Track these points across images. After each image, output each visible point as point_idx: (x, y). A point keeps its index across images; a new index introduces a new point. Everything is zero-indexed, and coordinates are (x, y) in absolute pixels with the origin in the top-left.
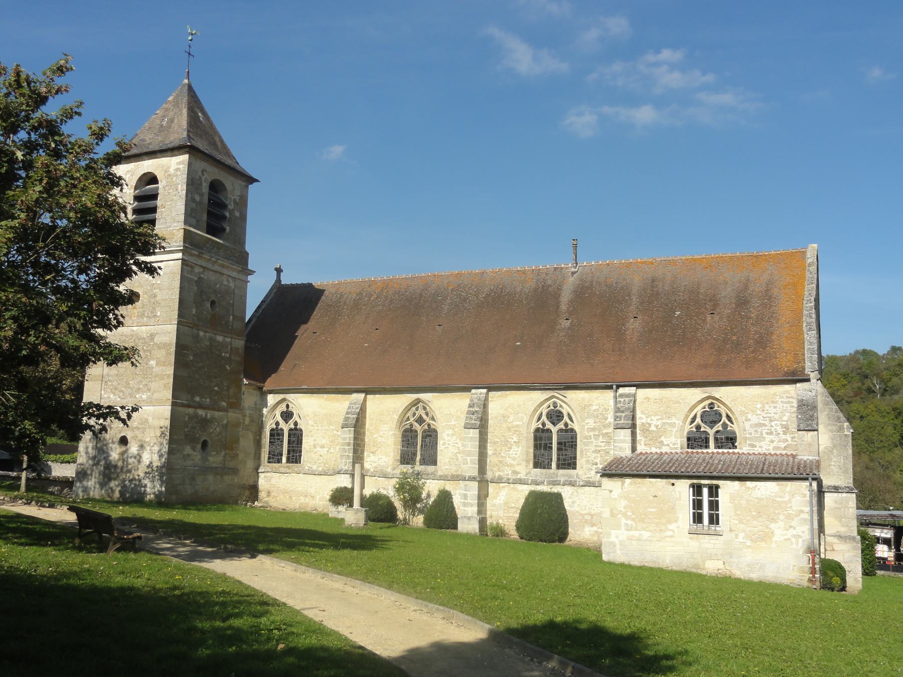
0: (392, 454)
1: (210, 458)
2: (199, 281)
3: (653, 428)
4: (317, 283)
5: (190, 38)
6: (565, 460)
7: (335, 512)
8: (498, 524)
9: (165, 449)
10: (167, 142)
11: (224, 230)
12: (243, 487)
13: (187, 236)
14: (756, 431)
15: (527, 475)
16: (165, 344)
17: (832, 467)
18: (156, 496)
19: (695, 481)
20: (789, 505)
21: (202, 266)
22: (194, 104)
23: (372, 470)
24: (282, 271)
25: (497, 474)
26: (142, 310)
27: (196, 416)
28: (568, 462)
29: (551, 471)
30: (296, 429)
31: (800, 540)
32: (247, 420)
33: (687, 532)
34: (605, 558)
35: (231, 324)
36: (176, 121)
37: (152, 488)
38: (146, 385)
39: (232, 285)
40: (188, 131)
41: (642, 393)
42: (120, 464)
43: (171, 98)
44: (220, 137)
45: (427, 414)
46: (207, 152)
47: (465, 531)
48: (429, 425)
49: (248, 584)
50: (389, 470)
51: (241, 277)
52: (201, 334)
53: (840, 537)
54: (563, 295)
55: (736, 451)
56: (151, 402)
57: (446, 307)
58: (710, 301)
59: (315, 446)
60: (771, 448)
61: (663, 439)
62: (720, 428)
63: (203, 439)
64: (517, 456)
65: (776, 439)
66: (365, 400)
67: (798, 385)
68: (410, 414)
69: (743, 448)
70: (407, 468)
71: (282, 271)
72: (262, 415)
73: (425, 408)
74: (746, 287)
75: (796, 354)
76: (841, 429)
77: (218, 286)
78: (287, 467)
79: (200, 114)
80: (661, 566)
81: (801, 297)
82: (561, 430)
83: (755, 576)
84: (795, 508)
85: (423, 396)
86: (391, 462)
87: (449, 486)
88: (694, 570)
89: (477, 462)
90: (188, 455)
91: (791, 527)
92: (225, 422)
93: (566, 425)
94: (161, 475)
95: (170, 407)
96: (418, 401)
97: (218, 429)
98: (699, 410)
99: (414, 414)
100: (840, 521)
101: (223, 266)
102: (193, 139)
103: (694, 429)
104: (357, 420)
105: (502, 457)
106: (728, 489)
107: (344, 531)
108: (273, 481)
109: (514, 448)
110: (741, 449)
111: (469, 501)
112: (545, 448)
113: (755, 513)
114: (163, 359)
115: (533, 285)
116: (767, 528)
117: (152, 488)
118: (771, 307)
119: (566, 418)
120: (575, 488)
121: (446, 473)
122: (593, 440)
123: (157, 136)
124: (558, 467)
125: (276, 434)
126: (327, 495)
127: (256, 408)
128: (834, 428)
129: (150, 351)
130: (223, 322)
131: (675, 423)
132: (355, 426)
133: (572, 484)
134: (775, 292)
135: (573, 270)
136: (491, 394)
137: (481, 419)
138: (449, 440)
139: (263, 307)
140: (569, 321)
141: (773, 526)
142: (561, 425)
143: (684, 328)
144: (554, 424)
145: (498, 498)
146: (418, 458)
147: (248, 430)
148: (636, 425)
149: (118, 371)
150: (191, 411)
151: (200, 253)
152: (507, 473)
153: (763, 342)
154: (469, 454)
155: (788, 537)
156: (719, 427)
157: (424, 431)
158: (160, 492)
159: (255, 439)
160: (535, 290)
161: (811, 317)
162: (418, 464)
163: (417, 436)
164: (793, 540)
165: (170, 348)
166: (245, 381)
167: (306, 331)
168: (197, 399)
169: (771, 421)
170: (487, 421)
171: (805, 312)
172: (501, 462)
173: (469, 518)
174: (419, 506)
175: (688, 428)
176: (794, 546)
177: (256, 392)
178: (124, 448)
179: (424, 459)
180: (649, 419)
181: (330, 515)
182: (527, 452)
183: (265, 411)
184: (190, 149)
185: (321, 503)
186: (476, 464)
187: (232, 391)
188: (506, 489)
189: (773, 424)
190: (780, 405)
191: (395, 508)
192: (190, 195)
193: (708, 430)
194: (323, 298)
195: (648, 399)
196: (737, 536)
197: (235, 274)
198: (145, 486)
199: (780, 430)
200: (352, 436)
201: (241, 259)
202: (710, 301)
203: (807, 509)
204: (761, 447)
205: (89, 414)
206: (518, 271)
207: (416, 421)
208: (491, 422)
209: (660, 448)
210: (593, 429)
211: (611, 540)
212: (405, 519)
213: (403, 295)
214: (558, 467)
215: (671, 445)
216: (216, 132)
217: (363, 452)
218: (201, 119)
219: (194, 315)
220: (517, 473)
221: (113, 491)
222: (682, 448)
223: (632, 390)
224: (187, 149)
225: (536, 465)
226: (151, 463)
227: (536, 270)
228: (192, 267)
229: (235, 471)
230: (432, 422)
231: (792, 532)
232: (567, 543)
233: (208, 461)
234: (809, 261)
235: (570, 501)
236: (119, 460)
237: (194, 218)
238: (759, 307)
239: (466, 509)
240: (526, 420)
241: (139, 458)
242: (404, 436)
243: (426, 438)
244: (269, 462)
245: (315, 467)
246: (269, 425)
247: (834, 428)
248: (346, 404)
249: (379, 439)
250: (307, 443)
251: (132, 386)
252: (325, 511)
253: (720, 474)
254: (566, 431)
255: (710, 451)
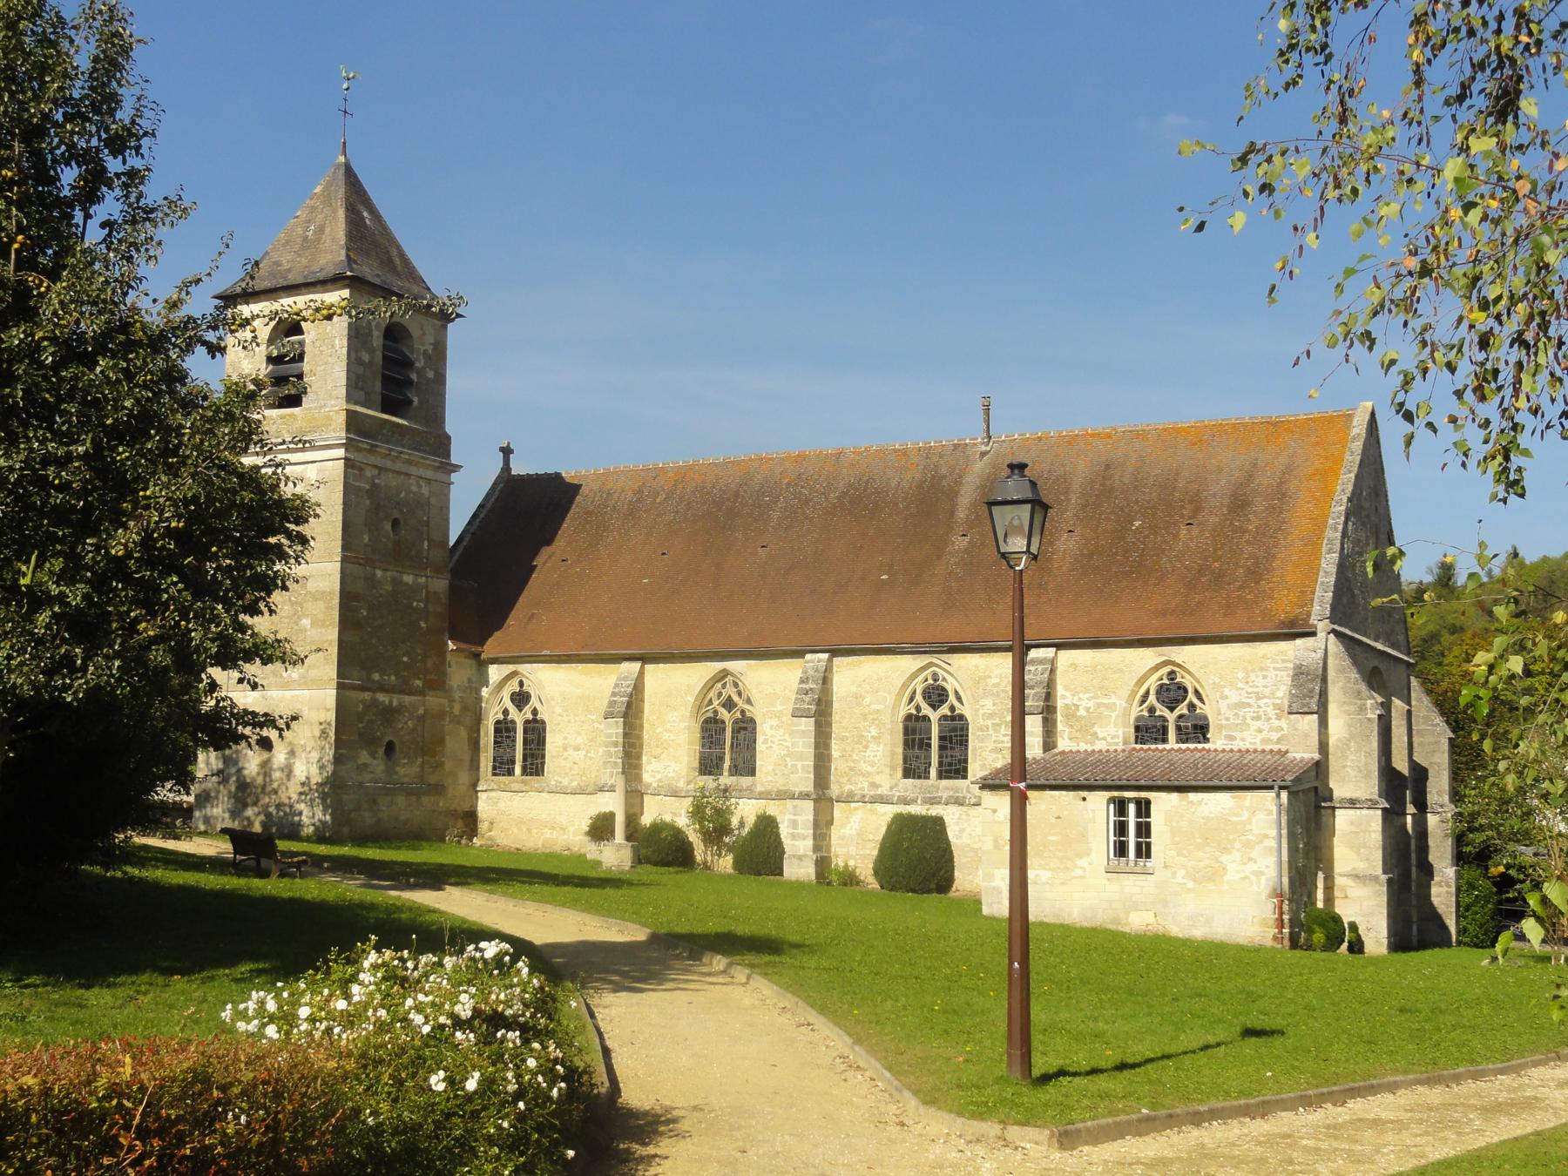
0: (685, 759)
1: (398, 769)
2: (373, 491)
3: (1082, 712)
4: (569, 474)
5: (345, 86)
6: (950, 764)
7: (592, 851)
8: (846, 866)
9: (330, 753)
10: (315, 268)
11: (410, 402)
12: (453, 814)
13: (353, 422)
14: (1236, 714)
15: (891, 788)
17: (1348, 769)
18: (317, 828)
19: (1116, 794)
20: (1248, 827)
21: (375, 467)
22: (356, 196)
23: (655, 785)
24: (512, 451)
25: (846, 788)
27: (375, 702)
28: (955, 768)
29: (930, 782)
30: (535, 720)
31: (1263, 879)
32: (457, 709)
33: (1103, 870)
34: (986, 910)
35: (425, 554)
36: (327, 230)
37: (311, 816)
39: (425, 491)
40: (348, 249)
41: (1066, 657)
42: (260, 780)
43: (318, 189)
44: (399, 247)
45: (740, 694)
46: (377, 281)
47: (794, 879)
48: (743, 712)
50: (681, 784)
51: (440, 476)
52: (379, 573)
53: (1356, 877)
54: (962, 492)
55: (1207, 746)
56: (305, 683)
57: (776, 515)
58: (1191, 502)
59: (565, 748)
60: (1258, 741)
61: (1096, 728)
62: (1185, 711)
63: (387, 739)
64: (876, 760)
65: (1266, 727)
66: (641, 673)
67: (1299, 642)
68: (712, 694)
69: (1217, 742)
70: (709, 782)
71: (512, 451)
72: (479, 699)
73: (736, 685)
74: (1250, 477)
75: (1302, 592)
76: (1362, 709)
77: (402, 495)
78: (523, 782)
79: (365, 214)
80: (1067, 920)
81: (1329, 495)
82: (944, 717)
83: (1198, 933)
84: (1256, 831)
85: (733, 665)
86: (684, 772)
87: (773, 809)
88: (1112, 927)
89: (812, 770)
90: (366, 765)
91: (1250, 859)
92: (421, 711)
93: (952, 708)
94: (324, 797)
95: (338, 565)
96: (725, 673)
97: (410, 723)
98: (1152, 683)
99: (720, 694)
100: (1358, 853)
101: (409, 462)
102: (355, 262)
103: (1146, 714)
104: (629, 705)
105: (853, 761)
106: (1162, 803)
107: (603, 876)
108: (501, 805)
109: (873, 747)
110: (1214, 742)
111: (800, 831)
112: (920, 747)
113: (1199, 840)
114: (321, 616)
115: (918, 476)
116: (1217, 861)
117: (311, 816)
118: (1281, 512)
119: (952, 698)
120: (965, 809)
121: (769, 788)
122: (991, 732)
123: (299, 256)
124: (941, 776)
125: (504, 729)
126: (585, 825)
127: (471, 688)
128: (1352, 708)
129: (301, 605)
130: (413, 553)
131: (1114, 704)
132: (625, 716)
133: (959, 802)
134: (1292, 487)
135: (984, 448)
136: (837, 661)
137: (819, 702)
139: (482, 516)
140: (967, 539)
141: (1225, 858)
142: (944, 710)
143: (1143, 550)
144: (934, 707)
145: (849, 826)
146: (727, 764)
147: (458, 723)
148: (1055, 708)
150: (367, 695)
151: (372, 445)
152: (861, 786)
153: (1257, 572)
154: (801, 757)
155: (1247, 874)
156: (1182, 709)
157: (736, 722)
158: (324, 823)
159: (470, 738)
160: (920, 485)
161: (1336, 530)
162: (726, 773)
163: (724, 729)
164: (1253, 878)
165: (332, 599)
166: (451, 645)
167: (550, 557)
168: (376, 676)
169: (1259, 698)
170: (829, 704)
171: (1331, 521)
172: (852, 769)
173: (800, 858)
174: (727, 840)
175: (1136, 711)
176: (1255, 888)
177: (473, 662)
178: (266, 755)
179: (735, 766)
180: (1076, 698)
181: (589, 857)
182: (893, 753)
183: (485, 692)
184: (355, 283)
185: (577, 838)
186: (809, 773)
187: (430, 663)
188: (860, 812)
189: (1261, 703)
190: (1272, 674)
191: (690, 844)
192: (353, 355)
193: (1167, 713)
194: (579, 499)
195: (1074, 666)
196: (1174, 874)
197: (429, 474)
198: (300, 814)
199: (1272, 713)
200: (621, 731)
201: (439, 445)
202: (1191, 502)
203: (1274, 833)
204: (1243, 740)
205: (244, 722)
206: (896, 451)
207: (724, 706)
208: (836, 706)
209: (1092, 743)
210: (991, 716)
211: (994, 884)
212: (705, 863)
213: (708, 493)
214: (941, 776)
215: (1109, 739)
216: (392, 241)
217: (639, 757)
218: (368, 222)
219: (366, 545)
220: (874, 785)
221: (251, 823)
222: (1125, 743)
223: (1049, 652)
224: (347, 282)
225: (908, 773)
226: (308, 778)
227: (925, 448)
228: (361, 469)
229: (439, 789)
230: (747, 707)
231: (1251, 867)
232: (952, 894)
233: (396, 773)
234: (1355, 431)
235: (957, 828)
236: (258, 774)
237: (362, 389)
238: (1263, 512)
239: (796, 843)
240: (890, 700)
241: (288, 771)
242: (704, 729)
243: (739, 732)
244: (494, 774)
245: (565, 782)
246: (492, 716)
247: (1352, 708)
248: (613, 680)
249: (666, 736)
250: (553, 742)
252: (583, 851)
253: (1150, 783)
254: (953, 718)
255: (1168, 746)
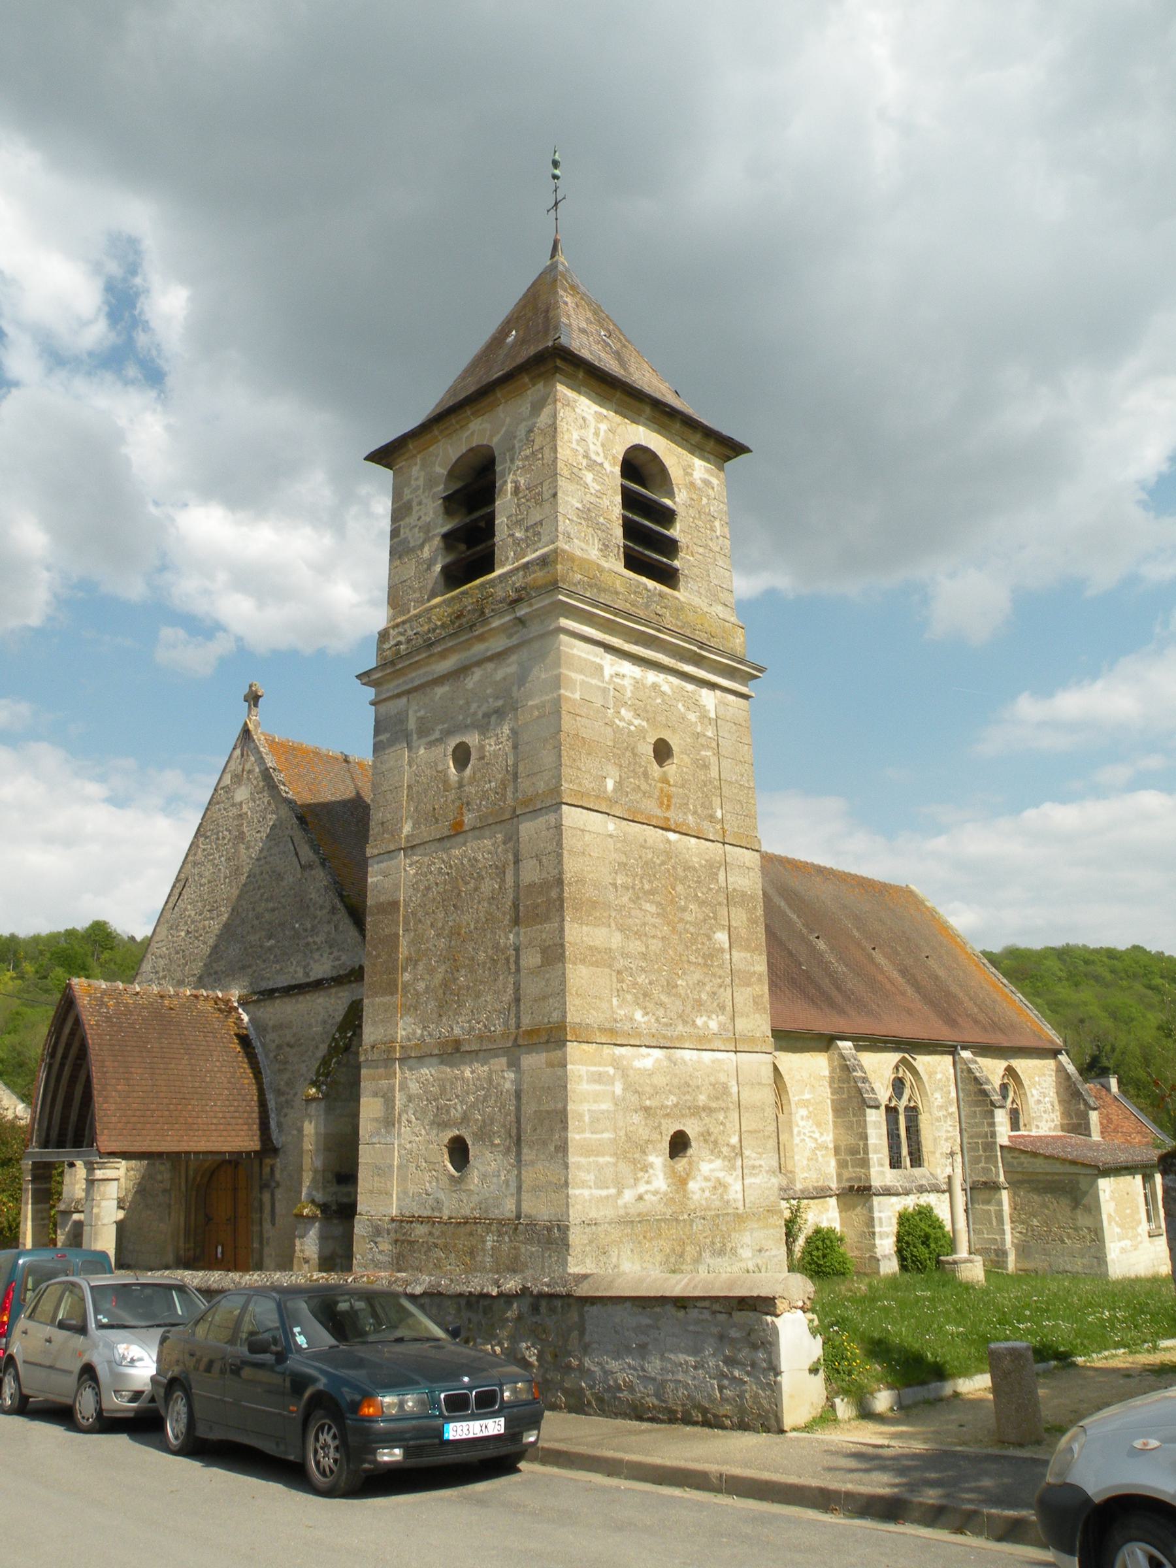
16: (744, 894)
26: (680, 790)
38: (714, 993)
49: (704, 1428)
138: (804, 1127)
149: (647, 947)
251: (682, 992)
